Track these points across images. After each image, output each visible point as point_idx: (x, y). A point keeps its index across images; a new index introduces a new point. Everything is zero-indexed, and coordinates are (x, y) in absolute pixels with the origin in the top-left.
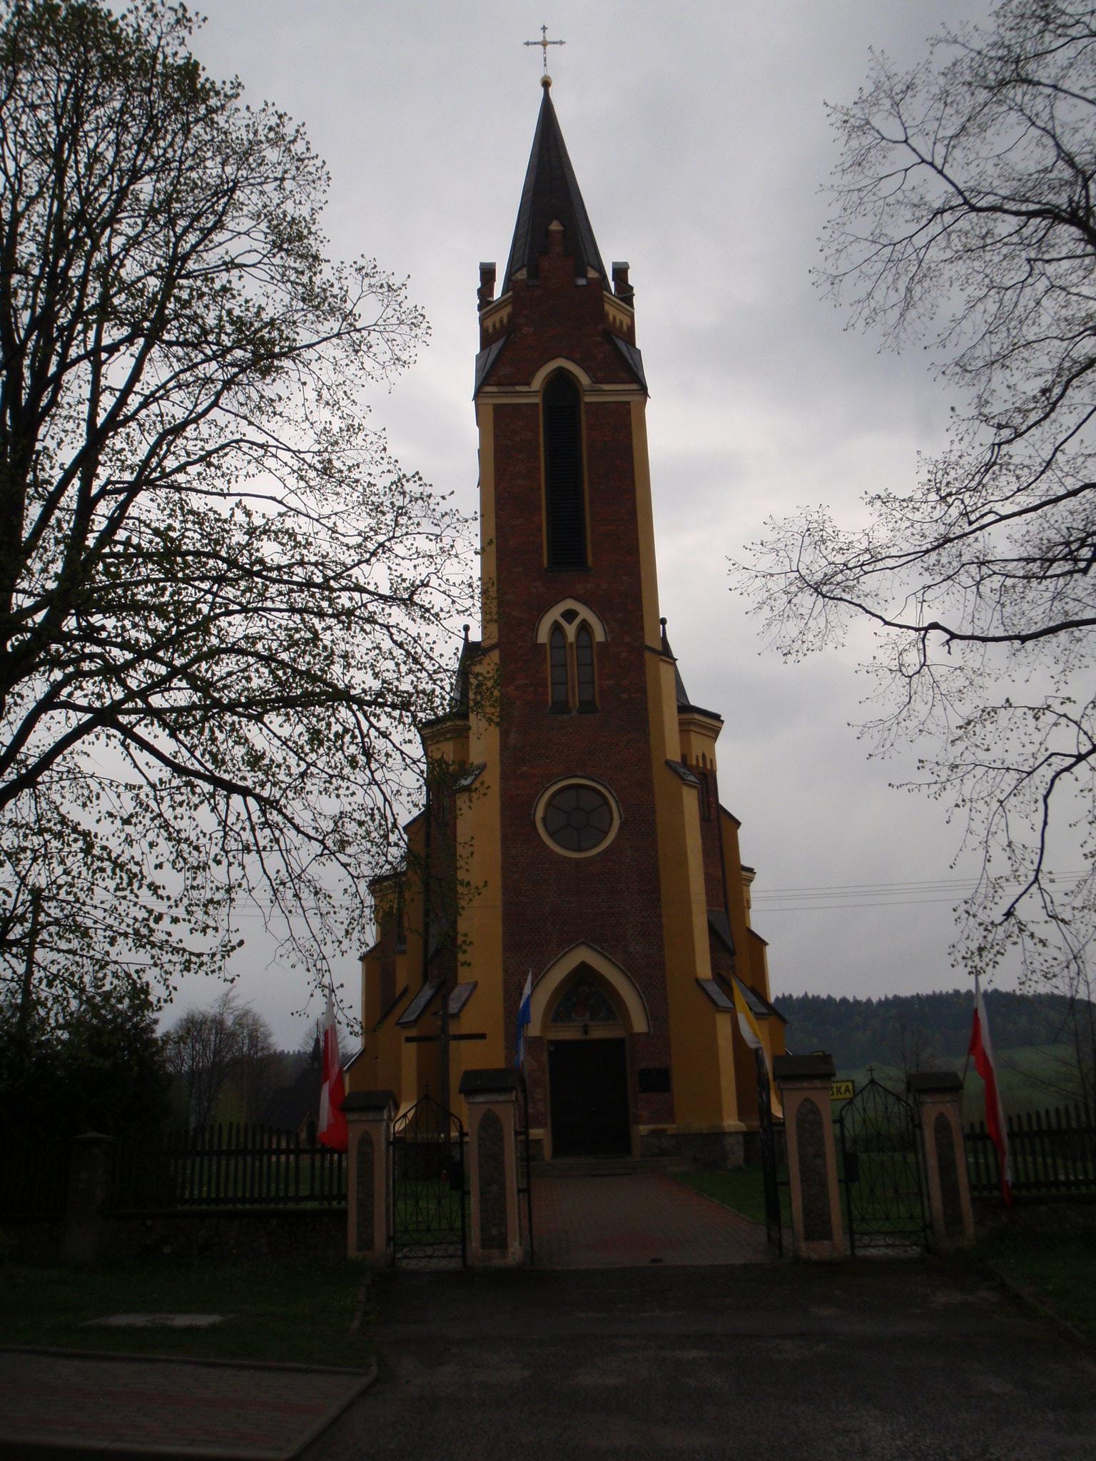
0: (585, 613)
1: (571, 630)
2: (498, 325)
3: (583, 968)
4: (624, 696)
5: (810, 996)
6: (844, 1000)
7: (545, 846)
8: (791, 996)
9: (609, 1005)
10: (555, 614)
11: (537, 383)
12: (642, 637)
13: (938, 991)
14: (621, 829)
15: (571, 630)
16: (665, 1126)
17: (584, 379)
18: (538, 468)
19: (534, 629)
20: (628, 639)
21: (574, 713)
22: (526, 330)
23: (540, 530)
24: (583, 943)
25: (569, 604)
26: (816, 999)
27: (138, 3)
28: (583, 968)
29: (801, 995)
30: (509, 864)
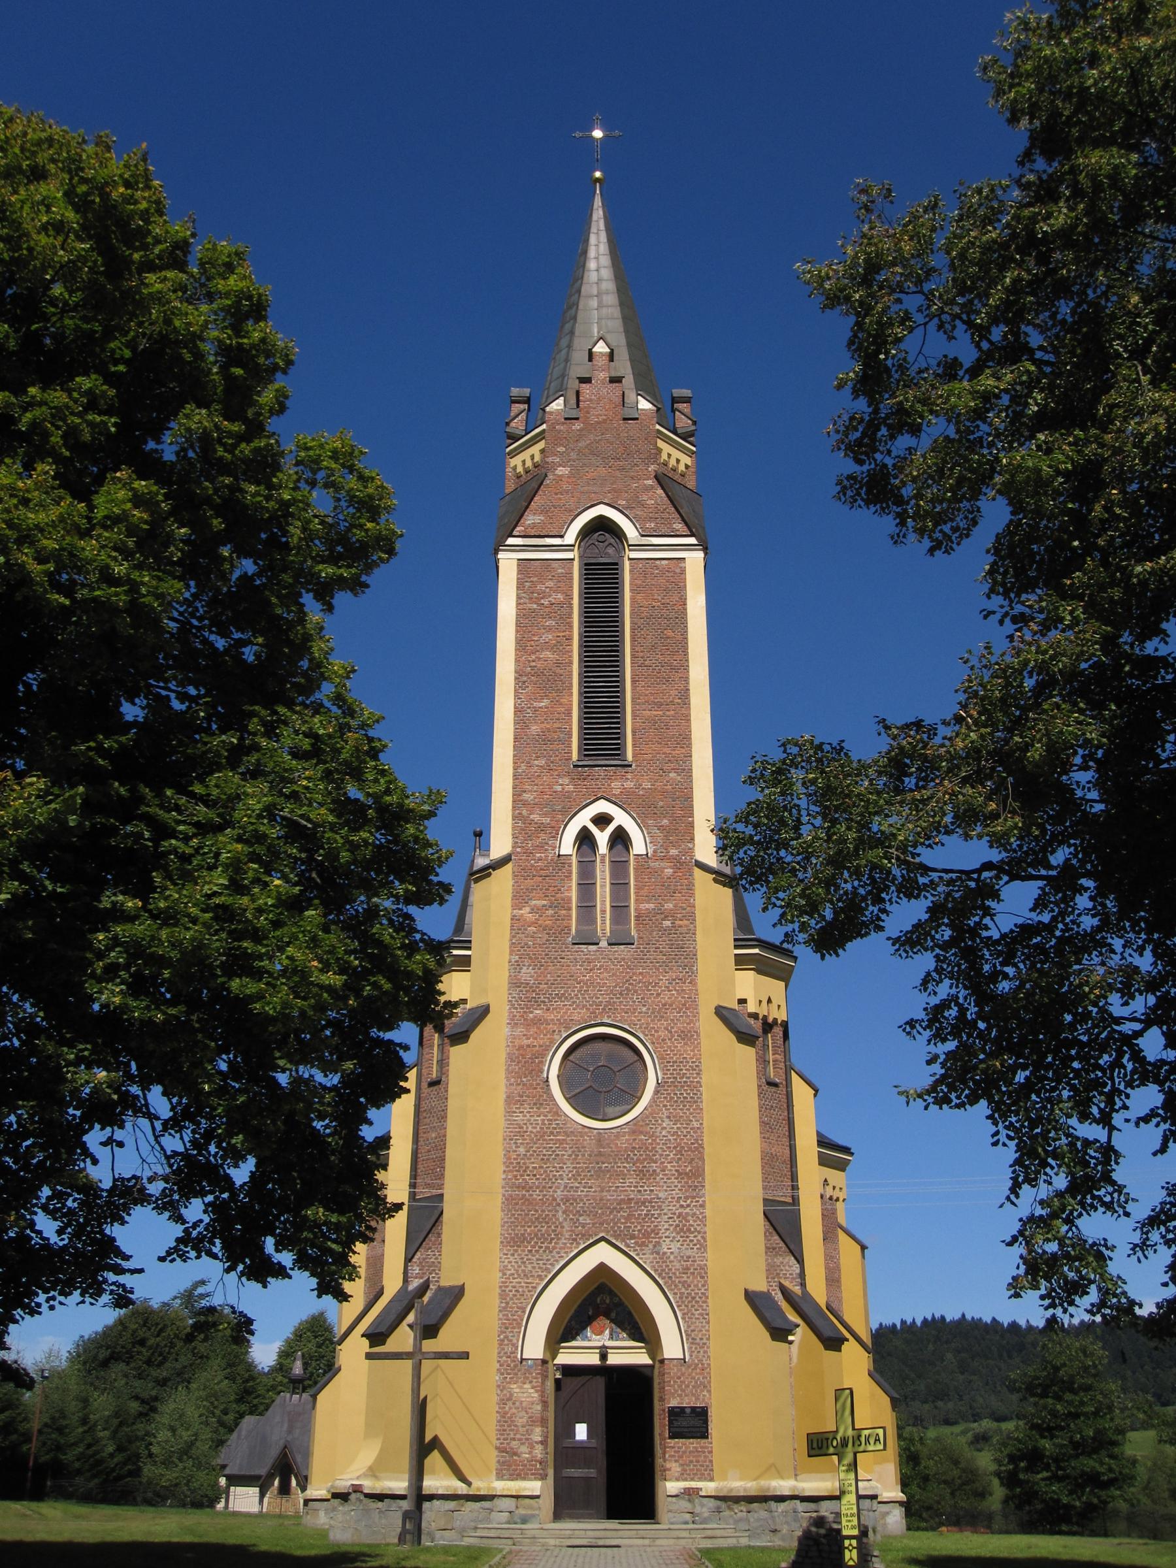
0: (621, 818)
1: (602, 838)
2: (529, 464)
3: (602, 1269)
4: (667, 923)
5: (968, 1317)
6: (1014, 1325)
7: (558, 1112)
8: (943, 1318)
9: (634, 1322)
10: (584, 818)
11: (571, 537)
12: (692, 850)
13: (304, 1318)
14: (656, 1092)
15: (602, 838)
16: (693, 1484)
17: (631, 531)
18: (570, 639)
19: (556, 833)
20: (674, 852)
21: (604, 944)
22: (561, 471)
23: (569, 714)
24: (603, 1239)
25: (602, 807)
26: (977, 1324)
27: (1142, 406)
28: (602, 1269)
29: (957, 1316)
30: (515, 1133)
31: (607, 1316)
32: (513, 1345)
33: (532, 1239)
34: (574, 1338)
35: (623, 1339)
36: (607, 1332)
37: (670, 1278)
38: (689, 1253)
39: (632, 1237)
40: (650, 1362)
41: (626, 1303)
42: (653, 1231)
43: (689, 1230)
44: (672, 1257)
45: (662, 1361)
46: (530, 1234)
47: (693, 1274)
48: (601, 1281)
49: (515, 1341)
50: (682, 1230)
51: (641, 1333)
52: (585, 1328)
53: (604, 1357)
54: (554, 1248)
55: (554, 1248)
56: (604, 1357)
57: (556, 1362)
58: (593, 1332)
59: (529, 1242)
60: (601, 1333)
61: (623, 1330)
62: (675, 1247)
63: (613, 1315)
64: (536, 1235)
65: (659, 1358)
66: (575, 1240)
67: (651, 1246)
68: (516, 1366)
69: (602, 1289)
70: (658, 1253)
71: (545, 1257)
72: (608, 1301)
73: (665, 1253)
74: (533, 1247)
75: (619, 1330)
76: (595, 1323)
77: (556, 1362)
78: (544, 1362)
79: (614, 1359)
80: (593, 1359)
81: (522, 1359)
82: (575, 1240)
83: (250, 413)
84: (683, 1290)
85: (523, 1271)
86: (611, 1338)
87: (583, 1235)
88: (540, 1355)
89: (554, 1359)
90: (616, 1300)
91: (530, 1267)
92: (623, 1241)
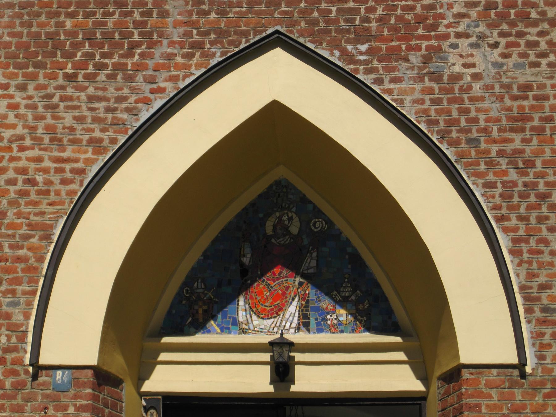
24: (277, 40)
31: (295, 267)
32: (13, 328)
33: (77, 46)
34: (199, 326)
35: (338, 328)
36: (293, 309)
37: (473, 142)
38: (526, 76)
39: (362, 36)
40: (417, 386)
41: (348, 232)
42: (420, 20)
43: (524, 17)
44: (477, 87)
45: (454, 375)
46: (72, 34)
47: (539, 131)
48: (280, 172)
49: (18, 317)
50: (503, 17)
51: (389, 312)
52: (232, 298)
53: (282, 372)
54: (138, 68)
55: (138, 68)
56: (282, 372)
57: (148, 386)
58: (253, 309)
59: (69, 56)
60: (276, 311)
61: (343, 302)
62: (485, 60)
63: (310, 264)
64: (90, 37)
65: (444, 366)
66: (198, 46)
67: (415, 59)
68: (18, 386)
69: (280, 195)
70: (436, 77)
71: (112, 92)
72: (294, 229)
73: (456, 78)
74: (82, 65)
75: (326, 303)
76: (259, 286)
77: (148, 386)
78: (102, 377)
79: (309, 380)
80: (255, 380)
81: (38, 369)
82: (198, 46)
83: (177, 46)
84: (513, 175)
85: (50, 129)
86: (304, 324)
87: (221, 34)
88: (88, 353)
89: (143, 375)
90: (318, 225)
91: (68, 119)
92: (335, 45)
